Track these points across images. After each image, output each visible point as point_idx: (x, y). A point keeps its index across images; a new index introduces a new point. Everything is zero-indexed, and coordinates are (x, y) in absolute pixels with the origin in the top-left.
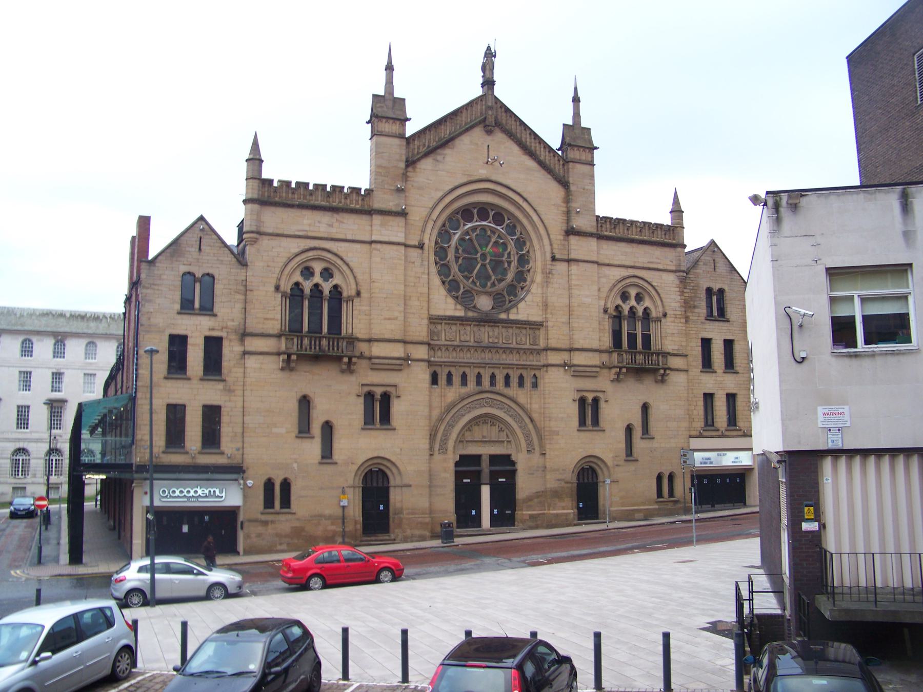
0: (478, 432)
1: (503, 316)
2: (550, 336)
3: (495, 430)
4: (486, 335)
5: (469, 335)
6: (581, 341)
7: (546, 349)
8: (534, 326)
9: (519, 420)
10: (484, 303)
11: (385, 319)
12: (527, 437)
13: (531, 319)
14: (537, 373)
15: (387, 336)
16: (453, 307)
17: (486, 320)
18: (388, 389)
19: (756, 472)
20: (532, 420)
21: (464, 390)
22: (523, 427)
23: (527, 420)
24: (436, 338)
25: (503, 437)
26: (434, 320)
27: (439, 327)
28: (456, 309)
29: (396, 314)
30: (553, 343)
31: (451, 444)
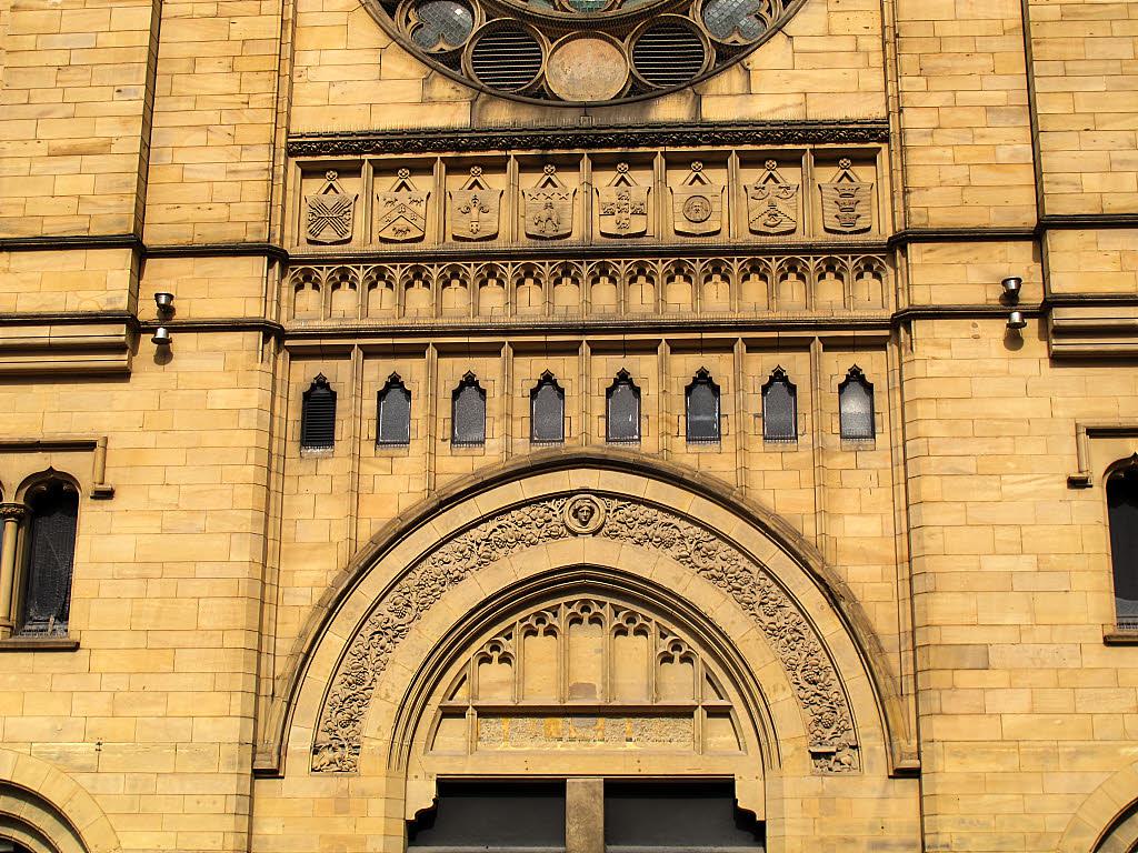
0: (542, 664)
1: (671, 110)
2: (915, 180)
3: (636, 652)
4: (586, 202)
5: (506, 205)
6: (1092, 182)
7: (899, 242)
8: (850, 144)
9: (762, 595)
10: (587, 71)
11: (54, 154)
12: (814, 681)
13: (820, 111)
14: (871, 364)
15: (52, 229)
16: (413, 90)
17: (611, 143)
18: (61, 462)
19: (561, 849)
20: (833, 598)
21: (457, 466)
22: (792, 633)
23: (811, 597)
24: (328, 234)
25: (680, 684)
26: (326, 156)
27: (350, 186)
28: (427, 101)
29: (105, 129)
30: (935, 209)
31: (377, 723)
